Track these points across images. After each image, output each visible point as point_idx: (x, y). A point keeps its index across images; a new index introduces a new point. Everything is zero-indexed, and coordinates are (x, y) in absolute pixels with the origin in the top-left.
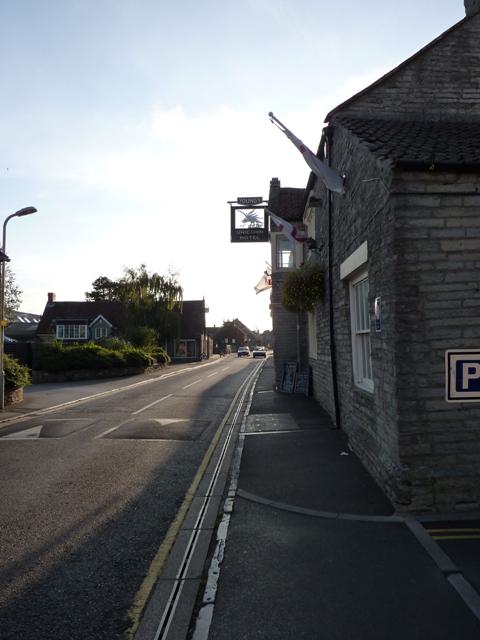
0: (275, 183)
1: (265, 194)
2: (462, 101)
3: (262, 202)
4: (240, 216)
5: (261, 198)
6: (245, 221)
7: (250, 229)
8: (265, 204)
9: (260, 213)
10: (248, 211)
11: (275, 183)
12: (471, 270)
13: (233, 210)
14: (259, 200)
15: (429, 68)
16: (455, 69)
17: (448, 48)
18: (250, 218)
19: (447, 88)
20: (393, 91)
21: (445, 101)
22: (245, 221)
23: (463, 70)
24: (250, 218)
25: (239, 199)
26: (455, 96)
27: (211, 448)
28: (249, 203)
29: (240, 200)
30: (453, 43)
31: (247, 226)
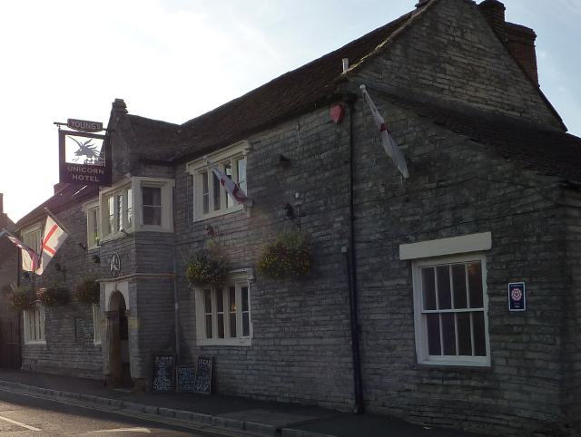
0: (119, 106)
1: (103, 117)
2: (435, 84)
3: (101, 129)
4: (72, 144)
5: (101, 124)
6: (79, 153)
7: (85, 166)
8: (103, 133)
9: (98, 144)
10: (83, 140)
11: (119, 106)
12: (311, 337)
13: (62, 134)
14: (98, 126)
15: (412, 45)
16: (429, 51)
17: (424, 28)
18: (85, 150)
19: (425, 69)
20: (389, 63)
21: (424, 81)
22: (79, 153)
23: (435, 53)
24: (85, 150)
25: (70, 121)
26: (446, 82)
27: (177, 330)
28: (83, 128)
29: (71, 123)
30: (427, 25)
31: (82, 160)
